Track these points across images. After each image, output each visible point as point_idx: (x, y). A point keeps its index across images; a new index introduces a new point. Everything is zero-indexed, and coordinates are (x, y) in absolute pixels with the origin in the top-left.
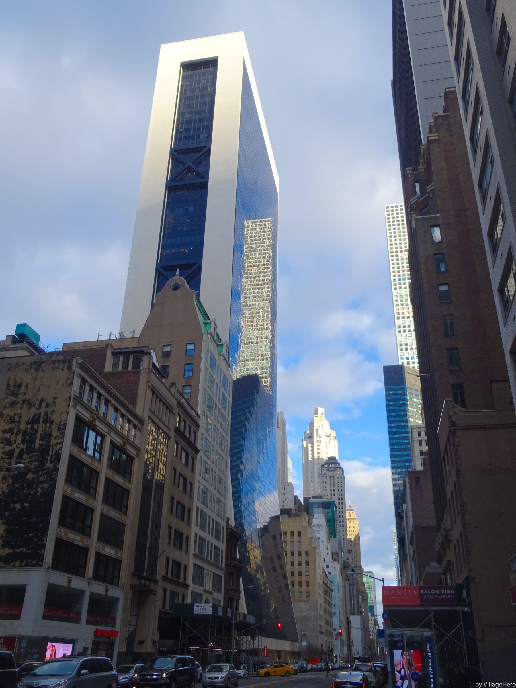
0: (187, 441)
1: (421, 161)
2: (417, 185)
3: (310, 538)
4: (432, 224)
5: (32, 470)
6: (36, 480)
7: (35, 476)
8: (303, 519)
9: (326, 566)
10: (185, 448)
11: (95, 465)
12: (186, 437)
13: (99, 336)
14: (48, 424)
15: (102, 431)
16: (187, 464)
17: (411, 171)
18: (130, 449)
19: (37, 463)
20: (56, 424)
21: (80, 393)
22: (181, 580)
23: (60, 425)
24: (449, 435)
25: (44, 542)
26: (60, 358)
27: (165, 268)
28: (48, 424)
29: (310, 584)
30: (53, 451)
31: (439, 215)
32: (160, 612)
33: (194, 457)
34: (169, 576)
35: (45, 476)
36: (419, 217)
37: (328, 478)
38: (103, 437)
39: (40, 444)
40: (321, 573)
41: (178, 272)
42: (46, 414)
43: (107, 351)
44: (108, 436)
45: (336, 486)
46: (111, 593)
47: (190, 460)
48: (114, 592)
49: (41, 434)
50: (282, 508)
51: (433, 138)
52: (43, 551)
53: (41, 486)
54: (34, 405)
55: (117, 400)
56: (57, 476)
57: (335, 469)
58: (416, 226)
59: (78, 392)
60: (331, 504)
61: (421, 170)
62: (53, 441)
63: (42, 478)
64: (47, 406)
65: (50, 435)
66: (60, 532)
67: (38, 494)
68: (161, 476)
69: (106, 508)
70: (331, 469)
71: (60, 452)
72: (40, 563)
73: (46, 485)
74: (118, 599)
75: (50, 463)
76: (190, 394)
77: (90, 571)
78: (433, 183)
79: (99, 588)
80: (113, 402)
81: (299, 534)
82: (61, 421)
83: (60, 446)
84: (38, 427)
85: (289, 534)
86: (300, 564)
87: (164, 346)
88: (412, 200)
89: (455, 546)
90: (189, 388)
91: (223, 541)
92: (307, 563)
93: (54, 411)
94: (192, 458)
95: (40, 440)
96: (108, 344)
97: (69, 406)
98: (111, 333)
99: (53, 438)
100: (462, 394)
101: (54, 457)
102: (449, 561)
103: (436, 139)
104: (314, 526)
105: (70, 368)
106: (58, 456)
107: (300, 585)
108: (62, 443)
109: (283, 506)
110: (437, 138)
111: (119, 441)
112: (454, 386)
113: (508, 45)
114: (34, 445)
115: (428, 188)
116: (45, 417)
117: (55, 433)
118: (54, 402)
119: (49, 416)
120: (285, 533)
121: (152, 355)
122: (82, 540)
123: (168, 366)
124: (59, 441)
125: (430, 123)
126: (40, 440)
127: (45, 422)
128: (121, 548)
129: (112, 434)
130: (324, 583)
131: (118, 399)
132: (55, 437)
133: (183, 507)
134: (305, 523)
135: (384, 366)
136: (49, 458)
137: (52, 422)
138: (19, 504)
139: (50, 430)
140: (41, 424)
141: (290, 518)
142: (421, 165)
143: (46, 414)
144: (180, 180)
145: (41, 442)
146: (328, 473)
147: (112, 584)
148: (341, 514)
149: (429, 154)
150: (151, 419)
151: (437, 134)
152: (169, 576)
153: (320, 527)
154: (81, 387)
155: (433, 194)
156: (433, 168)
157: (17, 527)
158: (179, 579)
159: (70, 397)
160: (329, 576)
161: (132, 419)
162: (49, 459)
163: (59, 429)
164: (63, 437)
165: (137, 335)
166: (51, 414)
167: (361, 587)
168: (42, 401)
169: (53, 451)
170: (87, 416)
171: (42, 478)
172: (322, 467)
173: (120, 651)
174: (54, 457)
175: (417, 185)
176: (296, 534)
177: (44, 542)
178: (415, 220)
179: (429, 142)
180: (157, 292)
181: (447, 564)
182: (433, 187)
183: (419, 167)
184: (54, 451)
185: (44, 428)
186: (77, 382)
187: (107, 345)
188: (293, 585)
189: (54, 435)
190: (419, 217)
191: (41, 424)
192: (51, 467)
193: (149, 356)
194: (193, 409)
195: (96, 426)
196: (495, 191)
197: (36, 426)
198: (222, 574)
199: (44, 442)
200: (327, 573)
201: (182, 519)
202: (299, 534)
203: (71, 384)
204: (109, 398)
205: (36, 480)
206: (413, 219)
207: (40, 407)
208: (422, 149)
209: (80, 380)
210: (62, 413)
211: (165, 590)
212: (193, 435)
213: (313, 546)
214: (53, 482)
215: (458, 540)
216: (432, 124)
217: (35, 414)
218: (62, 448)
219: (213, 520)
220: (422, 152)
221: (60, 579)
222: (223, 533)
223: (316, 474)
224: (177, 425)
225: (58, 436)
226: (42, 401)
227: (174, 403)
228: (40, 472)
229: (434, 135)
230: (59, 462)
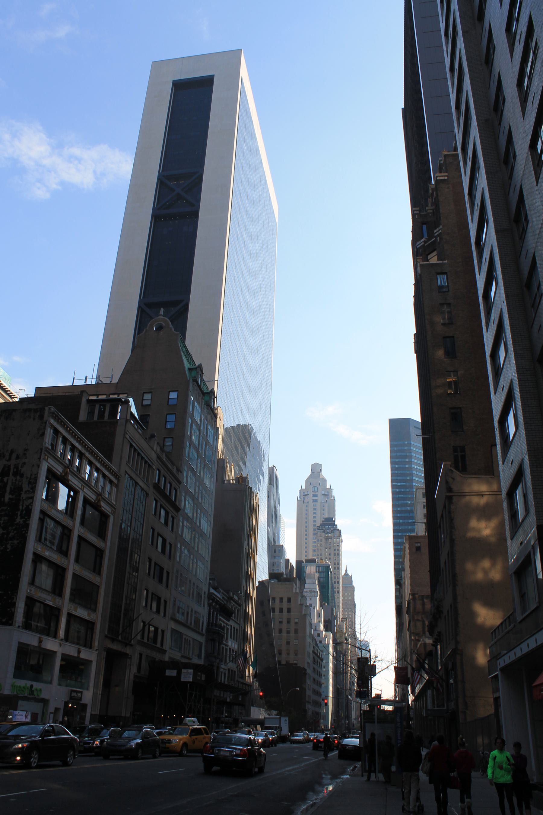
0: (167, 498)
1: (430, 200)
2: (425, 227)
3: (301, 604)
4: (439, 271)
5: (2, 525)
6: (5, 536)
7: (5, 531)
8: (294, 585)
9: (317, 635)
10: (164, 506)
11: (67, 522)
12: (166, 494)
13: (74, 380)
14: (18, 478)
15: (74, 486)
16: (166, 523)
17: (418, 212)
18: (104, 506)
19: (6, 518)
20: (27, 478)
21: (52, 445)
22: (158, 645)
23: (30, 478)
24: (445, 503)
25: (14, 600)
26: (32, 406)
27: (150, 305)
28: (18, 478)
29: (292, 610)
30: (23, 506)
31: (446, 262)
32: (135, 676)
33: (174, 516)
34: (145, 640)
35: (15, 532)
36: (424, 263)
37: (324, 541)
38: (76, 492)
39: (10, 499)
40: (311, 642)
41: (162, 311)
42: (16, 466)
43: (81, 398)
44: (81, 492)
45: (332, 549)
46: (83, 656)
47: (170, 519)
48: (85, 654)
49: (11, 488)
50: (272, 572)
51: (441, 178)
52: (13, 609)
53: (10, 542)
54: (4, 457)
55: (92, 452)
56: (27, 533)
58: (421, 272)
59: (50, 443)
61: (429, 211)
62: (24, 496)
63: (11, 534)
64: (18, 457)
65: (20, 489)
66: (30, 590)
67: (8, 550)
68: (138, 536)
69: (77, 567)
71: (30, 507)
72: (10, 622)
73: (16, 542)
74: (91, 661)
75: (21, 519)
76: (171, 447)
77: (62, 633)
78: (441, 227)
79: (71, 650)
80: (87, 454)
81: (289, 600)
82: (31, 475)
83: (30, 501)
84: (8, 480)
85: (277, 601)
86: (288, 632)
87: (144, 393)
88: (418, 243)
89: (445, 617)
90: (170, 440)
91: (204, 606)
92: (296, 631)
93: (24, 463)
94: (172, 517)
95: (10, 493)
96: (84, 389)
97: (40, 458)
98: (86, 377)
99: (23, 493)
100: (463, 457)
101: (24, 512)
102: (440, 632)
103: (445, 180)
104: (307, 592)
105: (41, 417)
106: (28, 512)
108: (32, 498)
109: (273, 570)
110: (446, 178)
111: (92, 497)
112: (455, 449)
113: (504, 103)
114: (4, 500)
115: (435, 231)
116: (15, 470)
117: (25, 487)
118: (25, 454)
119: (20, 468)
120: (274, 599)
121: (130, 404)
122: (89, 615)
123: (149, 415)
124: (30, 495)
125: (440, 160)
126: (10, 493)
127: (15, 474)
128: (95, 610)
129: (85, 490)
130: (313, 652)
131: (93, 451)
132: (26, 492)
133: (162, 569)
134: (296, 589)
136: (19, 513)
137: (22, 476)
138: (175, 675)
139: (20, 483)
140: (11, 477)
141: (279, 583)
142: (429, 205)
143: (16, 466)
144: (54, 538)
145: (11, 496)
146: (323, 535)
147: (85, 646)
149: (437, 194)
150: (129, 475)
151: (447, 174)
152: (145, 640)
153: (313, 594)
154: (53, 438)
155: (440, 239)
156: (441, 211)
158: (156, 644)
159: (41, 449)
160: (319, 645)
161: (107, 473)
162: (19, 515)
163: (30, 483)
164: (34, 492)
165: (115, 380)
166: (22, 467)
168: (12, 452)
169: (23, 506)
170: (59, 469)
171: (11, 534)
173: (93, 713)
174: (24, 512)
175: (425, 227)
176: (285, 600)
177: (14, 600)
178: (421, 265)
179: (437, 181)
180: (138, 334)
181: (437, 635)
182: (440, 231)
183: (427, 208)
184: (25, 506)
185: (14, 481)
186: (49, 432)
187: (82, 392)
188: (280, 654)
189: (24, 490)
190: (424, 263)
191: (11, 477)
192: (21, 522)
193: (127, 405)
194: (173, 464)
195: (68, 480)
196: (489, 253)
197: (5, 479)
198: (202, 639)
199: (14, 497)
200: (318, 642)
201: (160, 581)
202: (289, 600)
203: (43, 435)
204: (83, 451)
205: (5, 536)
206: (418, 264)
207: (10, 459)
208: (430, 188)
209: (52, 431)
210: (33, 465)
211: (141, 655)
212: (202, 473)
213: (303, 613)
214: (24, 539)
215: (448, 611)
216: (442, 162)
217: (5, 465)
218: (32, 503)
219: (194, 584)
220: (430, 191)
221: (31, 639)
222: (204, 597)
224: (157, 482)
225: (28, 491)
226: (12, 452)
227: (154, 456)
228: (10, 528)
229: (443, 174)
230: (29, 517)
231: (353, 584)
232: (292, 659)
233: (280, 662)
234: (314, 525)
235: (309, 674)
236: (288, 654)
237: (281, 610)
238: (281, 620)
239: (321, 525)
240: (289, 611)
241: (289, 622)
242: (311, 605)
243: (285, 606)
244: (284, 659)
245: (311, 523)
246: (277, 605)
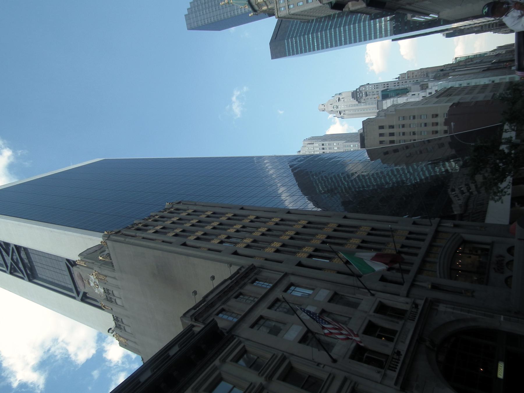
29: (392, 124)
37: (368, 97)
57: (361, 92)
60: (385, 93)
70: (361, 95)
81: (381, 127)
85: (382, 139)
107: (437, 124)
135: (273, 58)
148: (397, 84)
157: (501, 374)
167: (461, 64)
172: (359, 102)
188: (437, 132)
202: (381, 127)
223: (365, 107)
231: (406, 72)
232: (441, 120)
233: (446, 132)
234: (357, 105)
235: (472, 98)
236: (437, 124)
237: (392, 134)
238: (423, 125)
239: (357, 101)
240: (392, 127)
241: (403, 126)
242: (508, 89)
243: (386, 131)
244: (441, 128)
245: (357, 107)
246: (387, 138)
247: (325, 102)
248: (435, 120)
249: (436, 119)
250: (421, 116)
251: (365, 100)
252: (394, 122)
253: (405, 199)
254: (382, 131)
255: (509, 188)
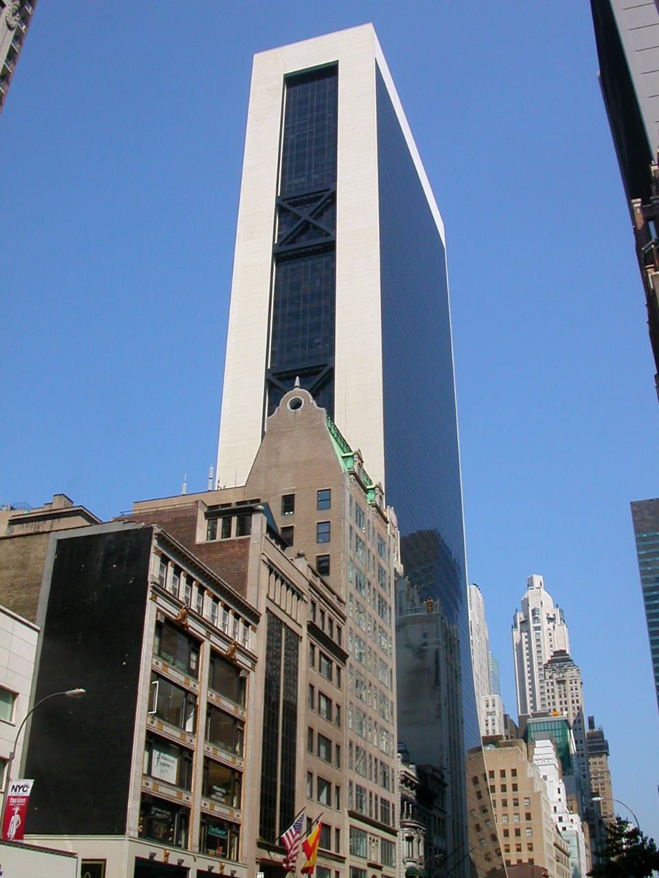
81: (514, 773)
172: (546, 667)
188: (508, 851)
202: (514, 773)
233: (508, 862)
236: (519, 850)
240: (515, 787)
246: (497, 781)
247: (607, 804)
248: (524, 847)
249: (526, 849)
250: (530, 828)
251: (551, 677)
252: (521, 793)
253: (415, 586)
254: (508, 774)
255: (428, 613)
